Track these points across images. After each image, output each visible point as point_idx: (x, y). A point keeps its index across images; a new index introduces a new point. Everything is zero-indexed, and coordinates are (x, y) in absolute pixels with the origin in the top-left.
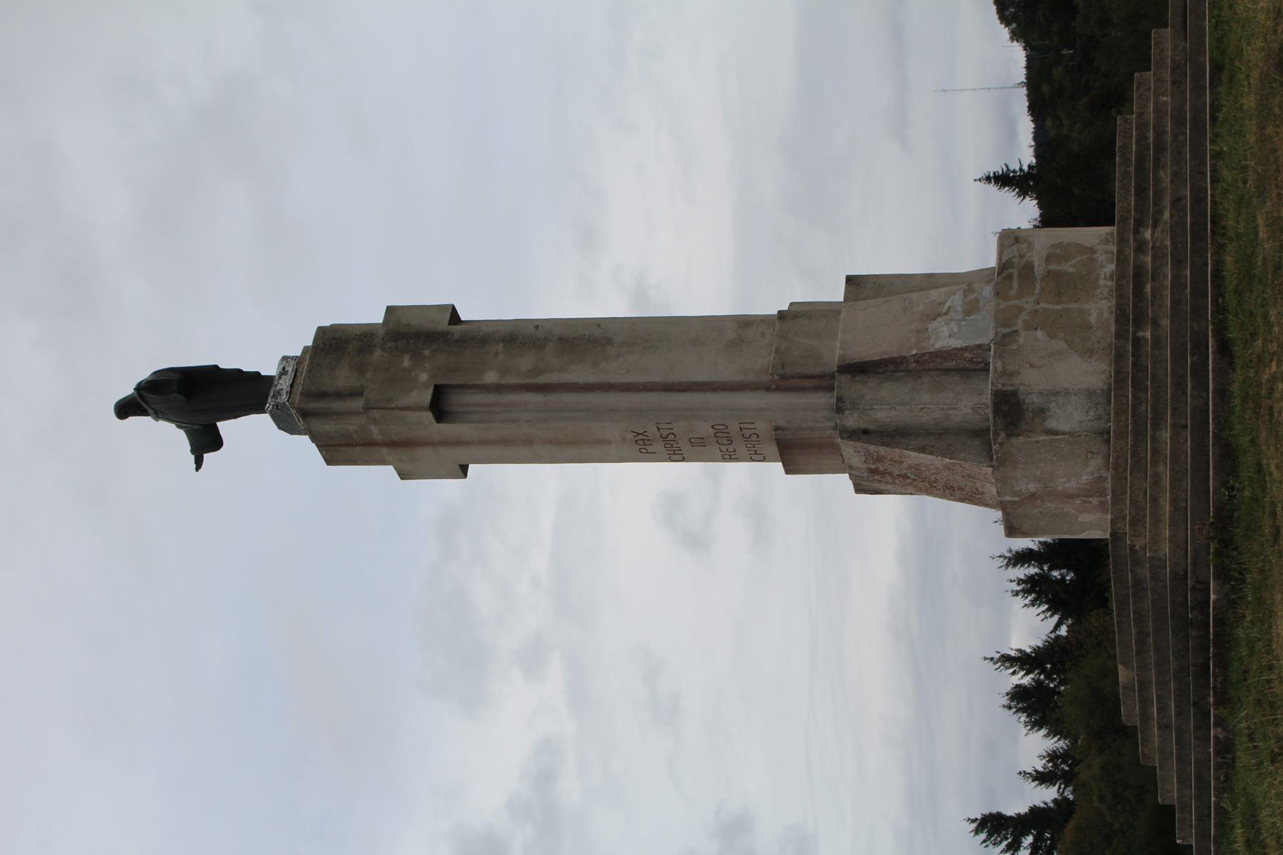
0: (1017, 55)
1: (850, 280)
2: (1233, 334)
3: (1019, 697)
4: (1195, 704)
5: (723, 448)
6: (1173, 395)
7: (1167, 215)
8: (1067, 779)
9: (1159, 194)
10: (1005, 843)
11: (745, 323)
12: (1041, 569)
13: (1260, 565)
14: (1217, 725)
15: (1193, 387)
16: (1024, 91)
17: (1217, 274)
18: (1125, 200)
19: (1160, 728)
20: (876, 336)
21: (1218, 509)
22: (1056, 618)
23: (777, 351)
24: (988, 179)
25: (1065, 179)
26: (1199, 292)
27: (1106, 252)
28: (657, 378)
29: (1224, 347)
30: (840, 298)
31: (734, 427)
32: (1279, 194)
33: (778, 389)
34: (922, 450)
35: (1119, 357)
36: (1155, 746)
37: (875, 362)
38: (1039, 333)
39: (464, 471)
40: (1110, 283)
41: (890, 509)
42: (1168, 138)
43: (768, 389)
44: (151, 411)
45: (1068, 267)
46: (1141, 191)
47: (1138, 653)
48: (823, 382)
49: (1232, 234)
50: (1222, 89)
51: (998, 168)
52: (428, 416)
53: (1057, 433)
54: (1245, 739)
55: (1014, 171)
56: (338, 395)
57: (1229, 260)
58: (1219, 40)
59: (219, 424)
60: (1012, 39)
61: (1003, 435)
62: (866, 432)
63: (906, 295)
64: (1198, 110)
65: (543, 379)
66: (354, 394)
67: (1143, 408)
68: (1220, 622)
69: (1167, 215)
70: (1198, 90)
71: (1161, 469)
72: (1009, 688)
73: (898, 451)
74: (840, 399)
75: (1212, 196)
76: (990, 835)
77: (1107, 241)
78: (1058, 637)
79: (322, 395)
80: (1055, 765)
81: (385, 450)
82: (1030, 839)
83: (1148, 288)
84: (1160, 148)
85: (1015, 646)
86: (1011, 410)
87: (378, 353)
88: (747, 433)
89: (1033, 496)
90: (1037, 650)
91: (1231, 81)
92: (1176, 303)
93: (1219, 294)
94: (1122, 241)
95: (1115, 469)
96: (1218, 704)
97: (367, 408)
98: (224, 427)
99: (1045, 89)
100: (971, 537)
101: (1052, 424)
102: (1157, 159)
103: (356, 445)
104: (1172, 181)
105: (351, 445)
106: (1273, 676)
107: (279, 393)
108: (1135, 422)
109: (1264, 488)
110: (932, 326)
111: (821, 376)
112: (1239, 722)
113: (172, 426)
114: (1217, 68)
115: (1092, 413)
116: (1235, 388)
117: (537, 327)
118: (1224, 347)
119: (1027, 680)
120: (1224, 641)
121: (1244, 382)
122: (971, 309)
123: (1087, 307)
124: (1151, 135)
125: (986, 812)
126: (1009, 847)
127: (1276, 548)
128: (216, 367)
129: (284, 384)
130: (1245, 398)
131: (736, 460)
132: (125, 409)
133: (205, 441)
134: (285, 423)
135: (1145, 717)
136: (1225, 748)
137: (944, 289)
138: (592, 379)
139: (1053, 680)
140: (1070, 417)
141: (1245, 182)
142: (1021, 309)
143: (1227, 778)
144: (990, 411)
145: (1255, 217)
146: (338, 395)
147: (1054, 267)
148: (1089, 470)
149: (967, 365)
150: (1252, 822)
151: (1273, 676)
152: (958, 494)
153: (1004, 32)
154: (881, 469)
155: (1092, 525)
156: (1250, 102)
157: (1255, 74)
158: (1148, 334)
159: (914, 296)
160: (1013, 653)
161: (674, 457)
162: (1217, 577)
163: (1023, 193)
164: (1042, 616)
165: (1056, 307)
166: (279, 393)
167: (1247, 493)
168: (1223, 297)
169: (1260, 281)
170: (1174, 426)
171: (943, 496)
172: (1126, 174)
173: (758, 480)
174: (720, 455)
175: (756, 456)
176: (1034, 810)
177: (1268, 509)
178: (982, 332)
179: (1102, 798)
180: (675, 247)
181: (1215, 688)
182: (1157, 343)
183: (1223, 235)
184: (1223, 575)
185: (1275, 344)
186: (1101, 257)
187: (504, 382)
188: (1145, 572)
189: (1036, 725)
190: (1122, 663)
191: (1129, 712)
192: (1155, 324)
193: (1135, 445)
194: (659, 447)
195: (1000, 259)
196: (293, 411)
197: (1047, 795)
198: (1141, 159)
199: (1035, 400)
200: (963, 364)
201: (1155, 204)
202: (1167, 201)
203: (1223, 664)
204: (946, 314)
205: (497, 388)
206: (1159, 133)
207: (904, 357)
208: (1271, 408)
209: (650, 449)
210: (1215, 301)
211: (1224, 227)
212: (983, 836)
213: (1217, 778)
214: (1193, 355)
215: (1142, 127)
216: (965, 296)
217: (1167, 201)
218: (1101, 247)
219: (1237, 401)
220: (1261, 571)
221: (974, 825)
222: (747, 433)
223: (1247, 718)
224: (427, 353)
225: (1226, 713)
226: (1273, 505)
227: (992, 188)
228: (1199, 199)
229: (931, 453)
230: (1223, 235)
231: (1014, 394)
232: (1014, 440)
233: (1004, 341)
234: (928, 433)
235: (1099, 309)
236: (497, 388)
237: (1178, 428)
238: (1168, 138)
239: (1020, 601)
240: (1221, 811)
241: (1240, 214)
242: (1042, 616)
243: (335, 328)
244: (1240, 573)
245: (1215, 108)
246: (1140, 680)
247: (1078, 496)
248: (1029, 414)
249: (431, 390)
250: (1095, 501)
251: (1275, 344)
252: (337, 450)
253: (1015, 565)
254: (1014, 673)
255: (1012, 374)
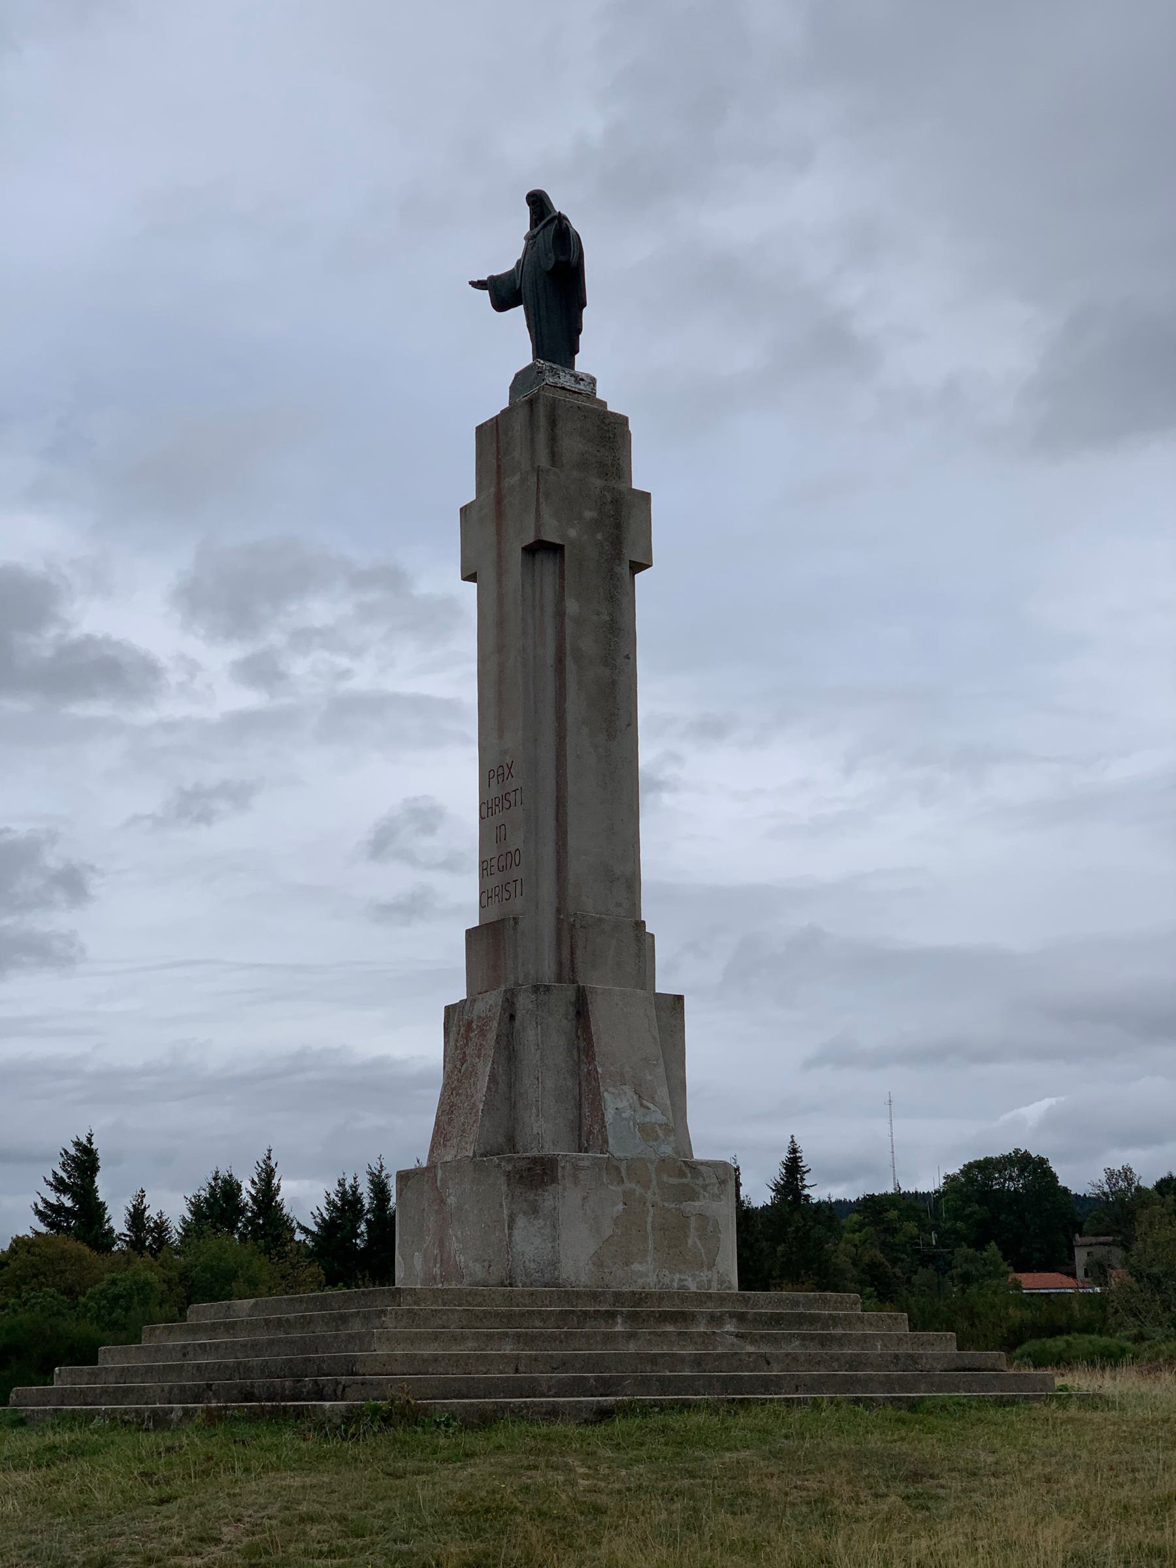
0: (928, 1182)
1: (679, 999)
2: (619, 1424)
3: (227, 1190)
4: (209, 1386)
5: (494, 862)
6: (551, 1356)
7: (751, 1349)
8: (136, 1244)
9: (774, 1340)
10: (64, 1175)
11: (632, 883)
12: (368, 1211)
13: (362, 1457)
14: (186, 1411)
15: (559, 1380)
16: (891, 1190)
17: (686, 1405)
18: (765, 1302)
19: (184, 1347)
20: (617, 1030)
21: (425, 1410)
22: (315, 1229)
23: (600, 920)
24: (794, 1151)
25: (792, 1238)
26: (665, 1385)
27: (710, 1281)
28: (571, 788)
29: (604, 1414)
30: (659, 990)
31: (517, 873)
32: (772, 1475)
33: (559, 922)
34: (493, 1078)
35: (594, 1296)
36: (163, 1341)
37: (589, 1027)
38: (621, 1207)
39: (469, 577)
40: (675, 1285)
41: (423, 1046)
42: (835, 1351)
43: (558, 911)
44: (535, 231)
45: (693, 1239)
46: (776, 1320)
47: (267, 1322)
48: (567, 970)
49: (730, 1422)
50: (890, 1411)
51: (806, 1161)
52: (530, 539)
53: (510, 1228)
54: (169, 1443)
55: (802, 1179)
56: (553, 439)
57: (700, 1418)
58: (944, 1408)
59: (521, 308)
60: (947, 1177)
61: (509, 1168)
62: (512, 1017)
63: (661, 1060)
64: (865, 1384)
65: (569, 662)
66: (554, 456)
67: (538, 1323)
68: (299, 1413)
69: (751, 1349)
70: (888, 1384)
71: (470, 1344)
72: (237, 1177)
73: (492, 1053)
74: (548, 989)
75: (771, 1400)
76: (73, 1159)
77: (721, 1282)
78: (293, 1231)
79: (553, 423)
80: (151, 1230)
81: (493, 490)
82: (68, 1203)
83: (670, 1328)
84: (824, 1341)
85: (282, 1183)
86: (538, 1174)
87: (598, 483)
88: (511, 888)
89: (443, 1202)
90: (279, 1207)
91: (898, 1420)
92: (653, 1359)
93: (662, 1407)
94: (722, 1299)
95: (470, 1293)
96: (208, 1411)
97: (538, 471)
98: (518, 314)
99: (893, 1214)
100: (404, 1138)
101: (521, 1222)
102: (812, 1338)
103: (498, 460)
104: (787, 1355)
105: (498, 453)
106: (238, 1473)
107: (555, 374)
108: (522, 1314)
109: (445, 1460)
110: (629, 1090)
111: (573, 969)
112: (188, 1437)
113: (520, 256)
114: (913, 1405)
115: (532, 1266)
116: (559, 1427)
117: (627, 657)
118: (604, 1414)
119: (245, 1197)
120: (278, 1417)
121: (566, 1437)
122: (647, 1131)
123: (649, 1259)
124: (839, 1331)
125: (100, 1154)
126: (60, 1180)
127: (381, 1475)
128: (584, 305)
129: (565, 380)
130: (548, 1438)
131: (482, 876)
132: (538, 202)
133: (503, 293)
134: (521, 381)
135: (195, 1330)
136: (160, 1421)
137: (668, 1102)
138: (570, 718)
139: (245, 1227)
140: (529, 1243)
141: (786, 1437)
142: (647, 1187)
143: (126, 1423)
144: (535, 1153)
145: (748, 1447)
146: (553, 439)
147: (693, 1222)
148: (471, 1264)
149: (586, 1129)
150: (77, 1451)
151: (238, 1473)
152: (445, 1118)
153: (955, 1169)
154: (472, 1035)
155: (410, 1266)
156: (875, 1442)
157: (905, 1447)
158: (619, 1328)
159: (661, 1070)
160: (275, 1181)
161: (485, 807)
162: (349, 1409)
163: (778, 1189)
164: (316, 1213)
165: (649, 1227)
166: (555, 374)
167: (442, 1442)
168: (659, 1413)
169: (678, 1454)
170: (518, 1357)
171: (441, 1103)
172: (796, 1304)
173: (461, 897)
174: (487, 858)
175: (487, 896)
176: (101, 1207)
177: (425, 1465)
178: (622, 1144)
179: (114, 1282)
180: (717, 809)
181: (226, 1408)
182: (609, 1338)
183: (729, 1412)
184: (351, 1417)
185: (607, 1471)
186: (704, 1275)
187: (567, 620)
188: (356, 1327)
189: (197, 1208)
190: (256, 1304)
191: (202, 1312)
192: (631, 1336)
193: (497, 1314)
194: (495, 791)
195: (703, 1163)
196: (535, 390)
197: (118, 1222)
198: (813, 1320)
199: (547, 1204)
200: (587, 1122)
201: (762, 1336)
202: (765, 1349)
203: (253, 1417)
204: (642, 1105)
205: (560, 614)
206: (840, 1341)
207: (594, 1059)
208: (536, 1467)
209: (494, 781)
210: (655, 1403)
211: (736, 1413)
212: (72, 1151)
213: (126, 1412)
214: (597, 1379)
215: (847, 1321)
216: (661, 1125)
217: (765, 1349)
218: (715, 1276)
219: (544, 1430)
220: (355, 1459)
221: (84, 1141)
222: (511, 888)
223: (191, 1444)
224: (599, 536)
225: (198, 1421)
226: (429, 1472)
227: (784, 1155)
228: (767, 1384)
229: (489, 1088)
230: (729, 1412)
231: (554, 1180)
232: (503, 1179)
233: (612, 1168)
234: (510, 1086)
235: (646, 1273)
236: (560, 614)
237: (515, 1362)
238: (835, 1351)
239: (333, 1187)
240: (90, 1416)
241: (751, 1431)
242: (316, 1213)
243: (626, 436)
244: (353, 1435)
245: (869, 1403)
246: (237, 1328)
247: (441, 1252)
248: (531, 1196)
249: (558, 541)
250: (437, 1270)
251: (607, 1471)
252: (491, 436)
253: (372, 1182)
254: (253, 1182)
255: (576, 1181)
